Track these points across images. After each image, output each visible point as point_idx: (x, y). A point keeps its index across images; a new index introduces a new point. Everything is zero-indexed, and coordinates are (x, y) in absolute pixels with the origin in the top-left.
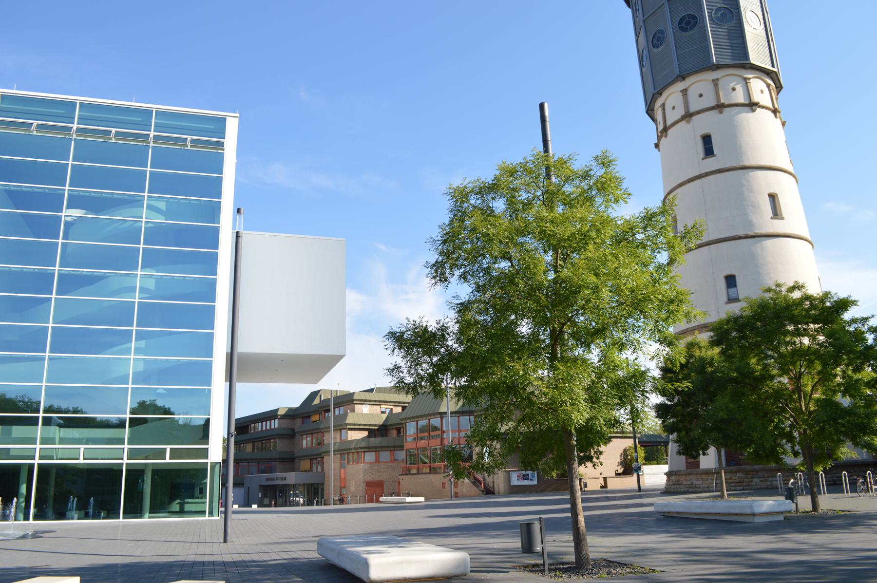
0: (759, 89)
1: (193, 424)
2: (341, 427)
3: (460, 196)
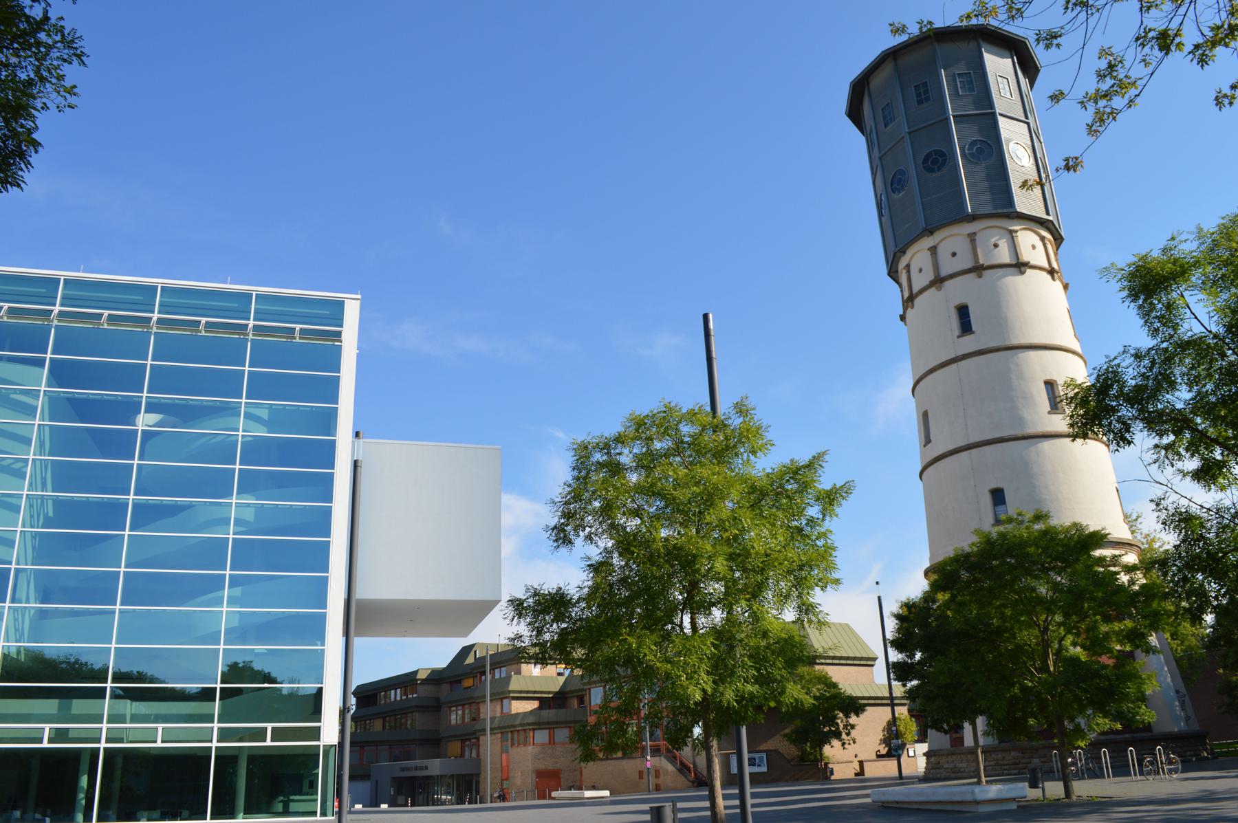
0: (1030, 244)
1: (301, 693)
2: (503, 695)
3: (583, 452)
